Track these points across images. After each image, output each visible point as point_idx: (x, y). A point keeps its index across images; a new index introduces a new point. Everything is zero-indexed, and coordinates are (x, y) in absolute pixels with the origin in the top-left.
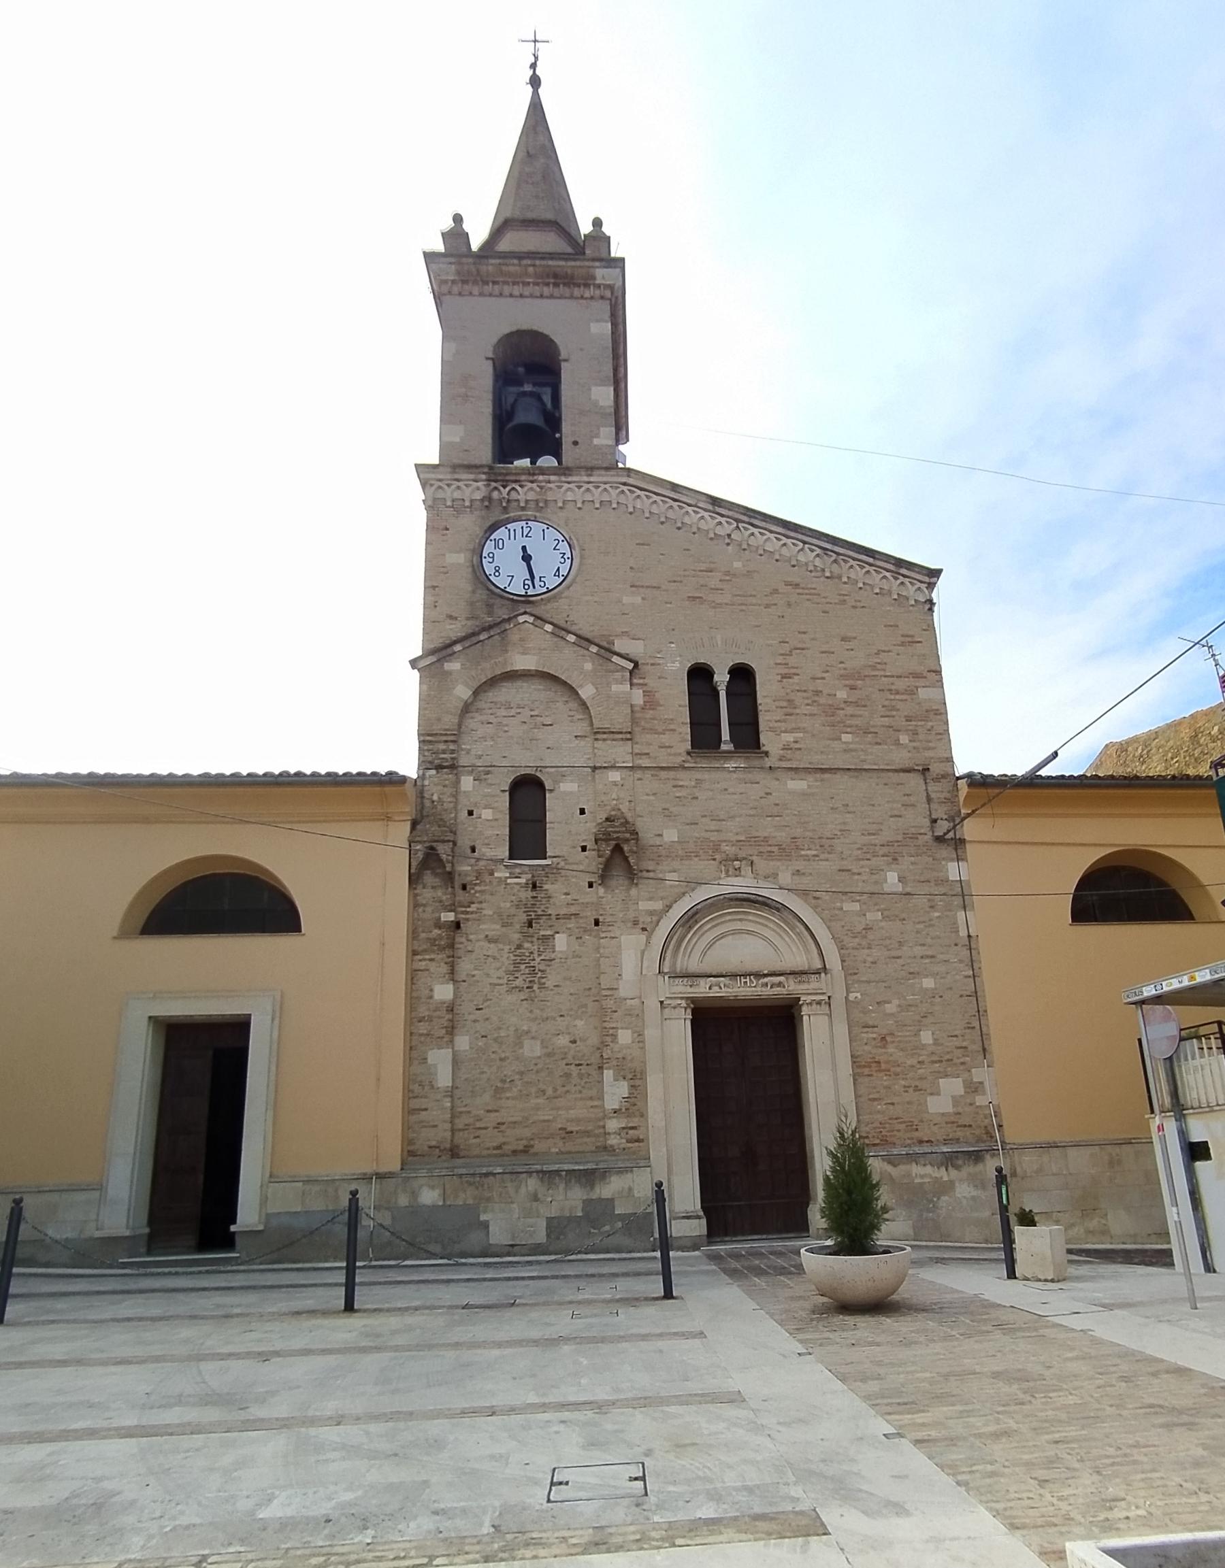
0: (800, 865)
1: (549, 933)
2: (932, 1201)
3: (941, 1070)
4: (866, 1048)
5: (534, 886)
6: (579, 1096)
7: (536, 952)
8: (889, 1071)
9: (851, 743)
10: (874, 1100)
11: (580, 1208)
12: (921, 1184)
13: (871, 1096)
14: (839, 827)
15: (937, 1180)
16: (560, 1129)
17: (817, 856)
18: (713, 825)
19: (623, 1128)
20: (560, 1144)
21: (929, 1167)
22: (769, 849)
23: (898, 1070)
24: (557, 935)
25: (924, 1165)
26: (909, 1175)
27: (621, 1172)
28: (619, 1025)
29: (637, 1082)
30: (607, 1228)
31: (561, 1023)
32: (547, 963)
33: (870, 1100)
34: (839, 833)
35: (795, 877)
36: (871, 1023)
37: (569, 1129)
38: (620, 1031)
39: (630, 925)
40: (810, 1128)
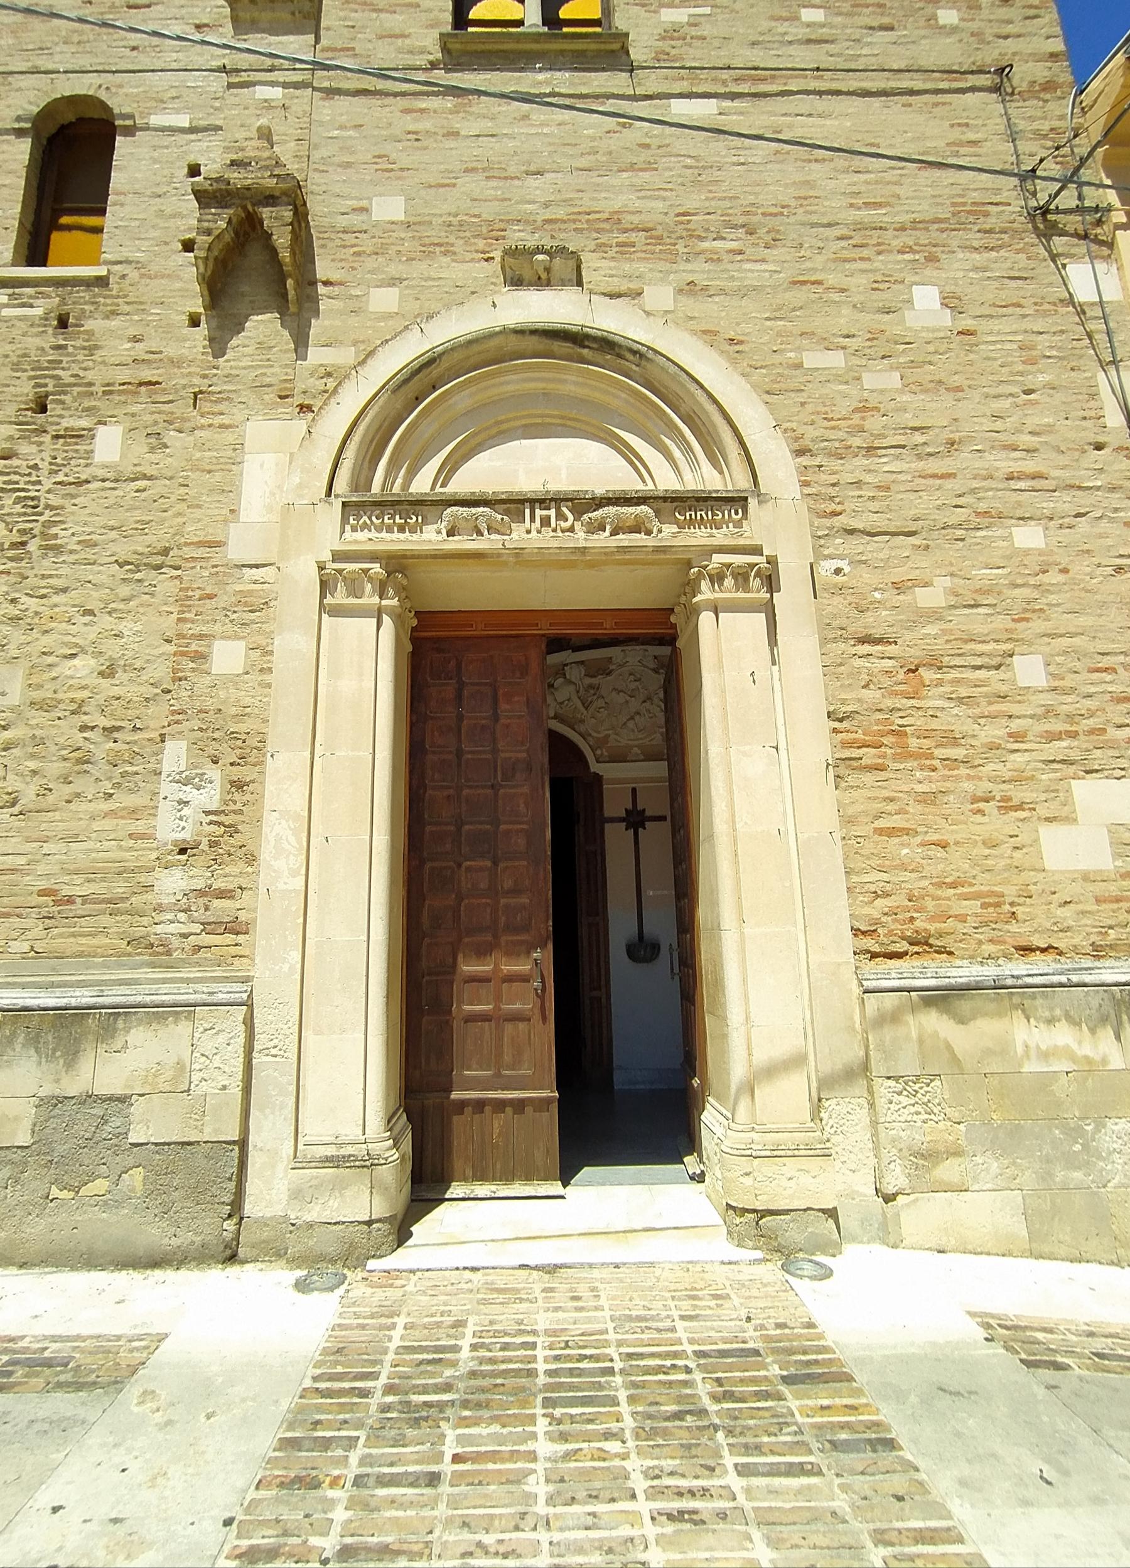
0: (698, 271)
1: (84, 423)
2: (1079, 1132)
3: (1075, 755)
4: (869, 695)
5: (63, 323)
6: (105, 806)
7: (44, 466)
8: (931, 757)
9: (823, 26)
10: (891, 832)
11: (27, 1124)
12: (1045, 1081)
13: (881, 823)
14: (792, 191)
15: (1090, 1068)
16: (43, 893)
17: (741, 253)
18: (492, 189)
19: (201, 893)
20: (38, 931)
21: (1063, 1027)
22: (623, 238)
23: (958, 753)
24: (101, 428)
25: (1051, 1021)
26: (1003, 1049)
27: (160, 1018)
28: (217, 628)
29: (246, 773)
30: (100, 1186)
31: (85, 632)
32: (72, 489)
33: (880, 832)
34: (793, 203)
35: (683, 299)
36: (877, 633)
37: (66, 891)
38: (218, 645)
39: (270, 397)
40: (715, 904)
